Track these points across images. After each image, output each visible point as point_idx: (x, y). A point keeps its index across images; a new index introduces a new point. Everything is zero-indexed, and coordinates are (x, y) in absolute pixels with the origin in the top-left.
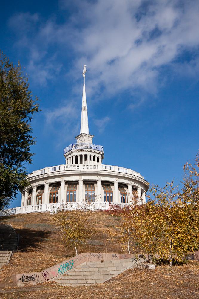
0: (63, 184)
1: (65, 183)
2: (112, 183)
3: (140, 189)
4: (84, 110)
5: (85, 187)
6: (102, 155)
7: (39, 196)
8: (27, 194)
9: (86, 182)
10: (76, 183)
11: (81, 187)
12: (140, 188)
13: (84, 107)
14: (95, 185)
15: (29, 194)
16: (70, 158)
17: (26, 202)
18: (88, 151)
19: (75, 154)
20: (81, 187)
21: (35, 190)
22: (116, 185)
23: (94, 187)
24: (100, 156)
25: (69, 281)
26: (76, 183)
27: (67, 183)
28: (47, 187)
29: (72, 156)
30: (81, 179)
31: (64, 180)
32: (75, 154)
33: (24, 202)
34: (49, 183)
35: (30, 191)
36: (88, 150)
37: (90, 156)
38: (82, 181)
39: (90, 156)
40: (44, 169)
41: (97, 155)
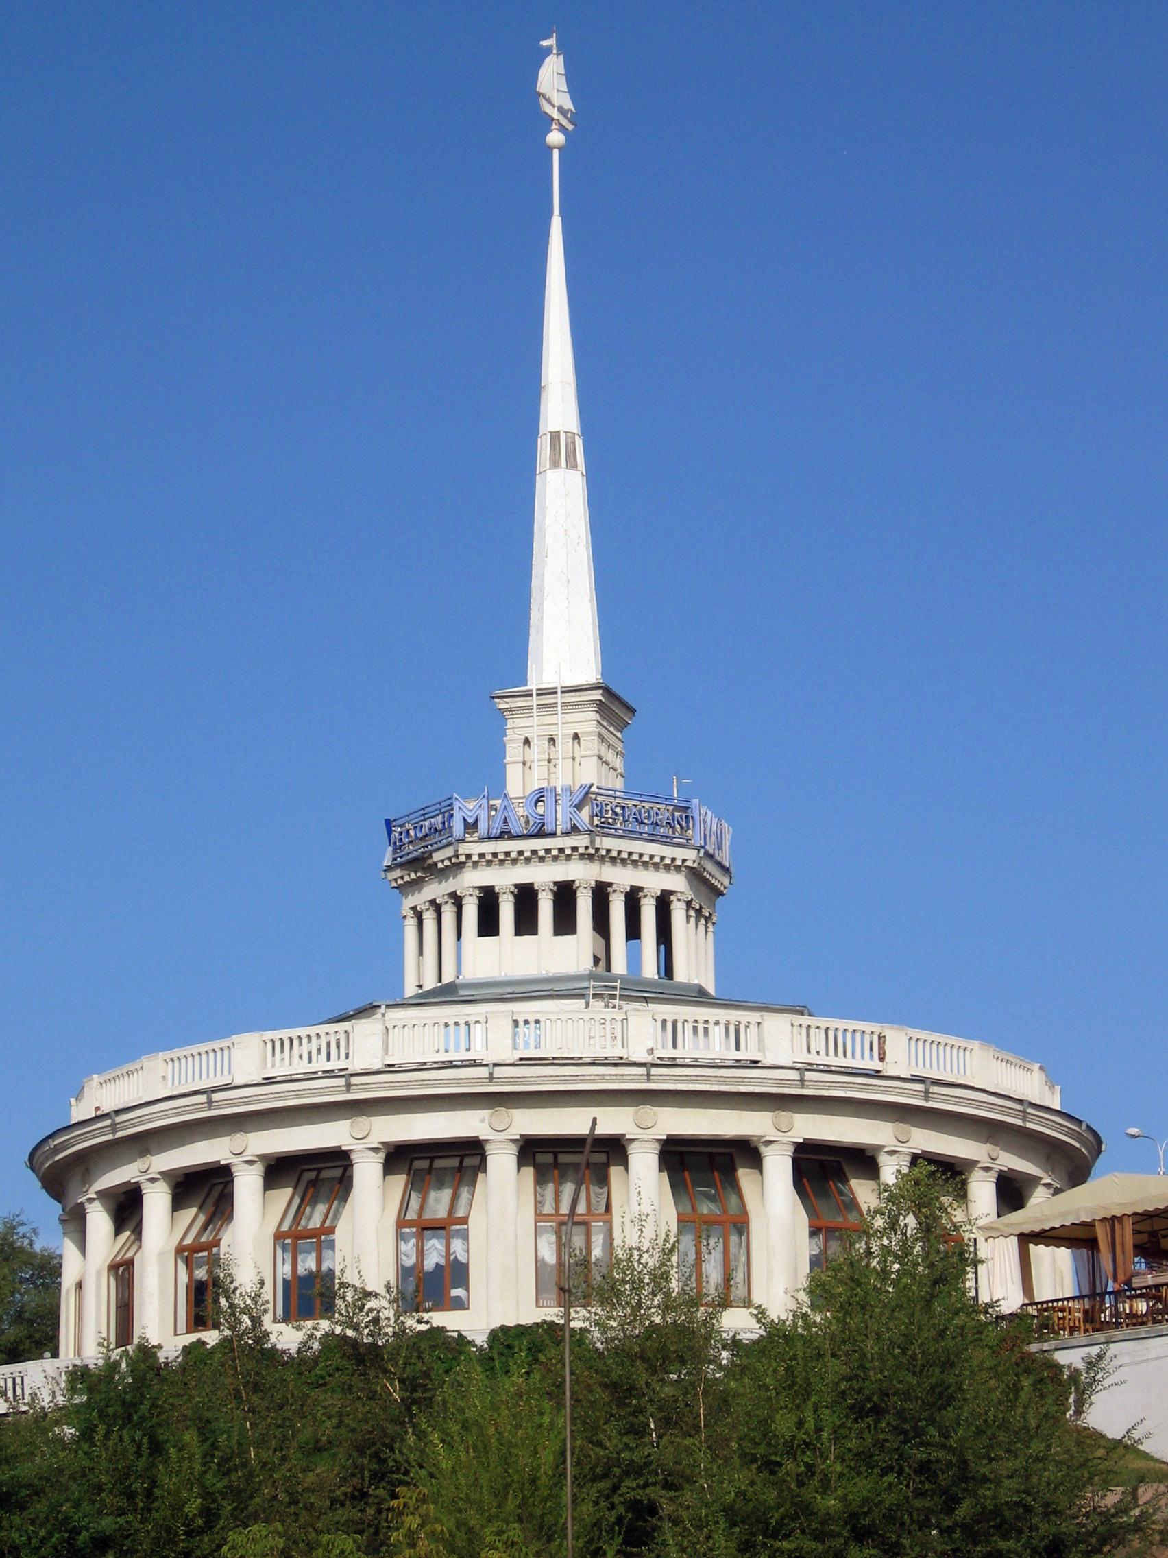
0: (367, 1171)
1: (381, 1156)
2: (746, 1152)
3: (992, 1176)
4: (555, 463)
5: (540, 1180)
6: (696, 876)
7: (196, 1248)
8: (99, 1221)
9: (536, 1153)
10: (465, 1157)
11: (504, 1190)
12: (987, 1169)
13: (555, 436)
14: (615, 1172)
15: (118, 1231)
16: (437, 907)
17: (98, 1309)
18: (582, 856)
19: (471, 880)
20: (504, 1190)
21: (157, 1201)
22: (778, 1168)
23: (604, 1180)
24: (677, 882)
25: (1055, 1293)
26: (465, 1157)
27: (398, 1157)
28: (247, 1186)
29: (457, 901)
30: (500, 1131)
31: (374, 1141)
32: (471, 880)
33: (79, 1285)
34: (263, 1157)
35: (127, 1208)
36: (574, 849)
37: (601, 893)
38: (513, 1149)
39: (601, 893)
40: (223, 1043)
41: (654, 882)
